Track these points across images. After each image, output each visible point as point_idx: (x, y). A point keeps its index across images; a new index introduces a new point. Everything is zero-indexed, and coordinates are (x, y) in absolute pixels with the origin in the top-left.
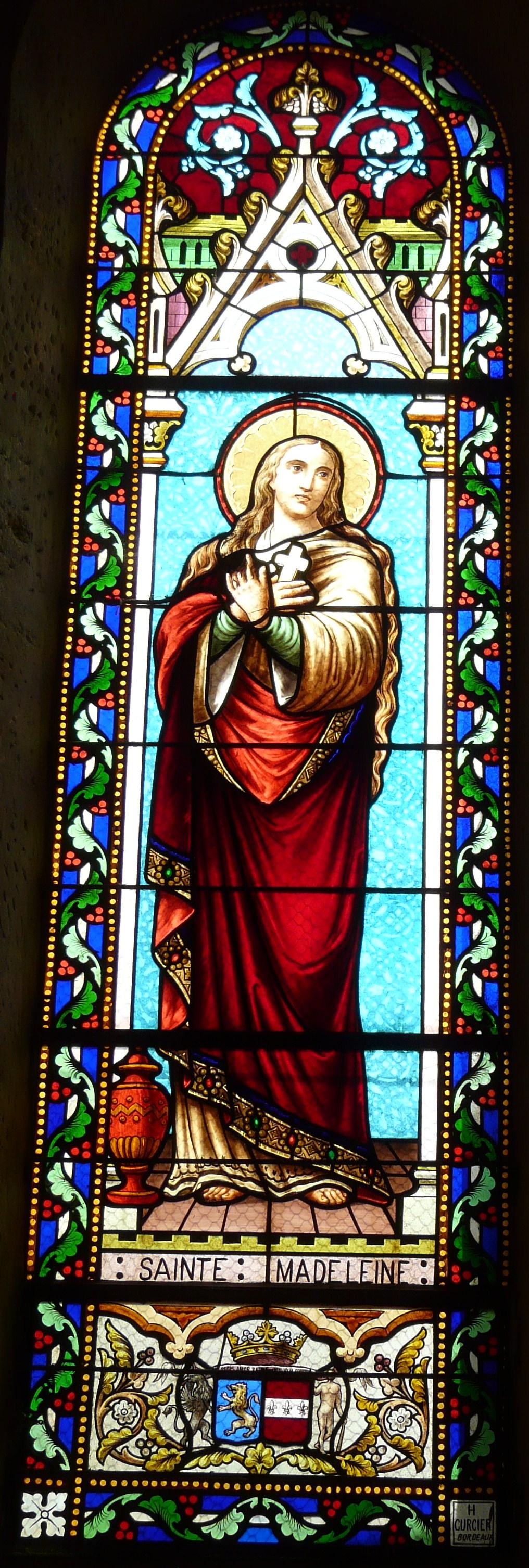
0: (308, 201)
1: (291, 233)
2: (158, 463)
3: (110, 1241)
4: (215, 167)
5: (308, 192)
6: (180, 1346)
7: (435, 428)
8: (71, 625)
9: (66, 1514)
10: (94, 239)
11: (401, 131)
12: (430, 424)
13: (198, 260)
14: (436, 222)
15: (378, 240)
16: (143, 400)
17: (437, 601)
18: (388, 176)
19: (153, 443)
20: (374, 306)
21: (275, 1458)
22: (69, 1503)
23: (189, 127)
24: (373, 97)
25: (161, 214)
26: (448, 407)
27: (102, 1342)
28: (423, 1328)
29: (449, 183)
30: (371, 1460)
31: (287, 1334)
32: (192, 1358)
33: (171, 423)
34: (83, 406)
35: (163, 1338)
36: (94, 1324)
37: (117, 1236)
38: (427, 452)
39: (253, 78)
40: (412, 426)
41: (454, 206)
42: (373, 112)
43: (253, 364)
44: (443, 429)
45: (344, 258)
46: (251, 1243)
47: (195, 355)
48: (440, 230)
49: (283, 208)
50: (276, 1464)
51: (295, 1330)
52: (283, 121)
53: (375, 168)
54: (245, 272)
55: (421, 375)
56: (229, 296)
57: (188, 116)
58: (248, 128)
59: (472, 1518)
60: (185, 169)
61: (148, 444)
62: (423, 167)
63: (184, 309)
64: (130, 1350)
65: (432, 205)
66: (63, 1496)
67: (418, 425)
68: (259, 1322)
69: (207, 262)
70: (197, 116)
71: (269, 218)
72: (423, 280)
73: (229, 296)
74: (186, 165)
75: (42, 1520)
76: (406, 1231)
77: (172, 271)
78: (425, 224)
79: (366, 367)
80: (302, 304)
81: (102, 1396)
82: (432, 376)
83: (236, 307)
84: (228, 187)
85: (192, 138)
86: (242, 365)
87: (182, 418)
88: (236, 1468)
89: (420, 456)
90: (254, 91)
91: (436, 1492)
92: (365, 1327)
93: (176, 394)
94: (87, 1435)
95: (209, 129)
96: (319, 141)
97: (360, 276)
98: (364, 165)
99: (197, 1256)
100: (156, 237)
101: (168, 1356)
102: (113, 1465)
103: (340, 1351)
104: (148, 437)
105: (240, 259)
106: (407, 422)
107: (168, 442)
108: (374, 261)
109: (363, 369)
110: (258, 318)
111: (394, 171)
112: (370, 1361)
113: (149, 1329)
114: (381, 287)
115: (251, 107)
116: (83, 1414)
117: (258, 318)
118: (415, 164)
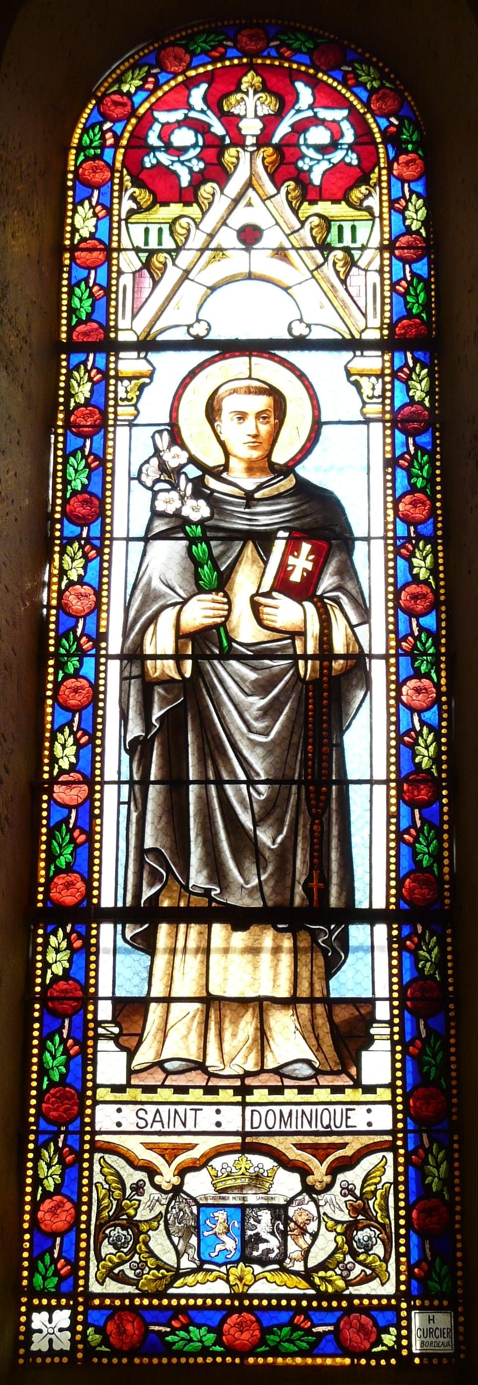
0: (254, 189)
1: (240, 218)
2: (131, 415)
3: (103, 1094)
4: (173, 162)
5: (254, 182)
6: (167, 1176)
7: (373, 379)
8: (34, 1107)
9: (72, 1329)
10: (42, 834)
11: (334, 128)
12: (369, 376)
13: (160, 243)
14: (366, 203)
15: (316, 221)
16: (116, 362)
17: (380, 774)
18: (325, 165)
19: (126, 399)
20: (313, 277)
21: (255, 1276)
22: (73, 1318)
23: (150, 128)
24: (310, 100)
25: (128, 204)
26: (384, 361)
27: (98, 1178)
28: (384, 1157)
29: (376, 170)
30: (341, 1275)
31: (260, 1166)
32: (177, 1190)
33: (142, 380)
34: (59, 498)
35: (152, 1171)
36: (91, 1160)
37: (329, 1090)
38: (367, 400)
39: (204, 87)
40: (353, 378)
41: (381, 188)
42: (310, 113)
43: (209, 330)
44: (380, 380)
45: (288, 236)
46: (226, 1095)
47: (158, 323)
48: (369, 210)
49: (233, 197)
50: (255, 1281)
51: (268, 1163)
52: (231, 120)
53: (312, 159)
54: (202, 250)
55: (357, 336)
56: (186, 273)
57: (147, 121)
58: (200, 128)
59: (432, 1325)
60: (148, 165)
61: (122, 400)
62: (354, 156)
63: (147, 282)
64: (121, 1181)
65: (363, 189)
66: (67, 1313)
67: (358, 378)
68: (236, 1156)
69: (168, 243)
70: (156, 120)
71: (221, 204)
72: (356, 254)
73: (186, 273)
74: (149, 161)
75: (49, 1336)
76: (366, 1081)
77: (137, 250)
78: (358, 207)
79: (308, 329)
80: (250, 276)
81: (100, 1227)
82: (366, 336)
83: (193, 280)
84: (185, 180)
85: (153, 139)
86: (199, 330)
87: (151, 376)
88: (221, 1288)
89: (361, 405)
90: (205, 99)
91: (396, 1139)
92: (330, 1159)
93: (146, 355)
94: (87, 1259)
95: (167, 130)
96: (263, 140)
97: (301, 252)
98: (303, 157)
99: (188, 1107)
100: (123, 223)
101: (158, 1188)
102: (112, 1287)
103: (310, 1179)
104: (122, 394)
105: (197, 240)
106: (349, 374)
107: (138, 397)
108: (314, 238)
109: (305, 331)
110: (213, 289)
111: (329, 160)
112: (336, 1189)
113: (141, 1163)
114: (320, 260)
115: (203, 112)
116: (84, 1231)
117: (213, 289)
118: (347, 154)
